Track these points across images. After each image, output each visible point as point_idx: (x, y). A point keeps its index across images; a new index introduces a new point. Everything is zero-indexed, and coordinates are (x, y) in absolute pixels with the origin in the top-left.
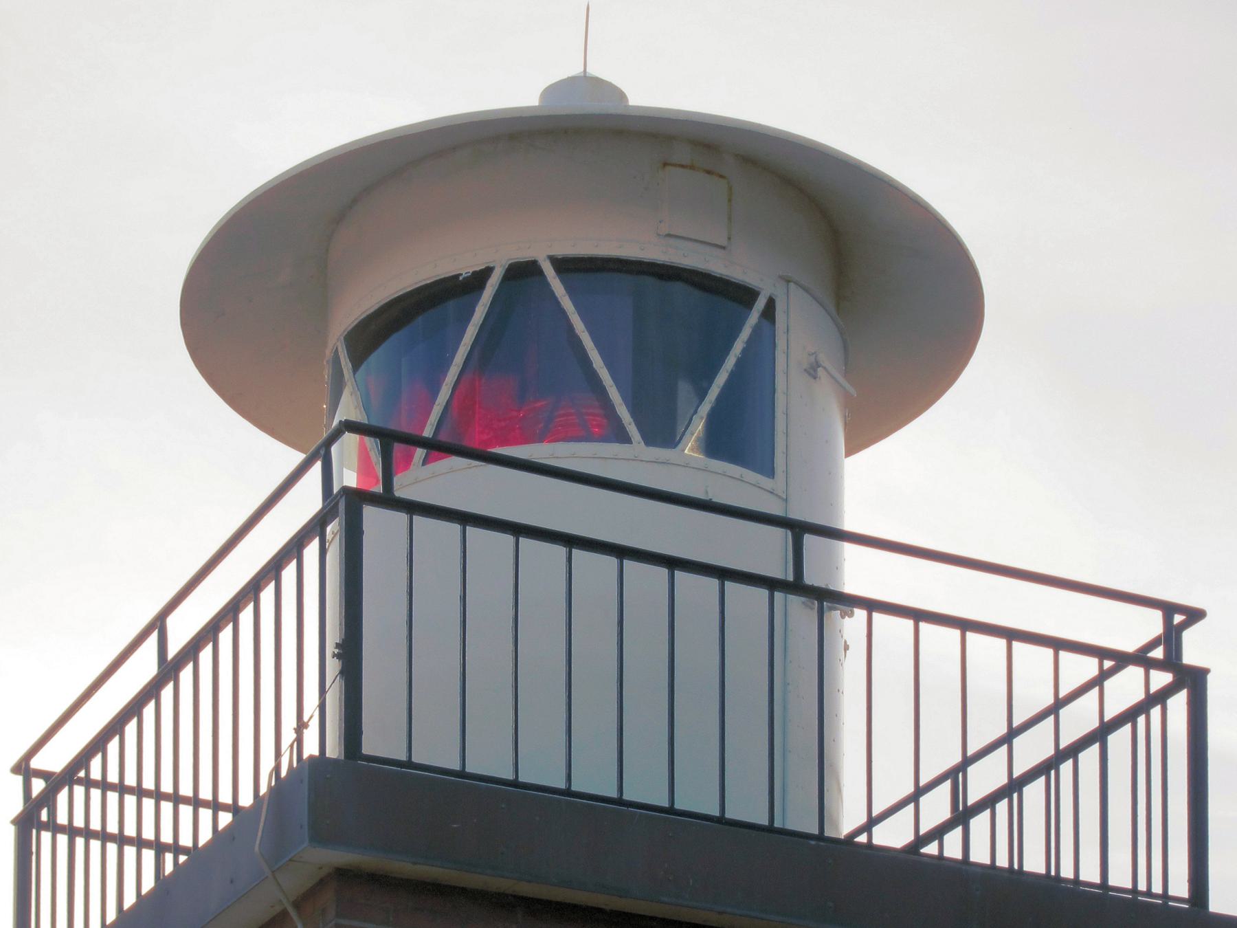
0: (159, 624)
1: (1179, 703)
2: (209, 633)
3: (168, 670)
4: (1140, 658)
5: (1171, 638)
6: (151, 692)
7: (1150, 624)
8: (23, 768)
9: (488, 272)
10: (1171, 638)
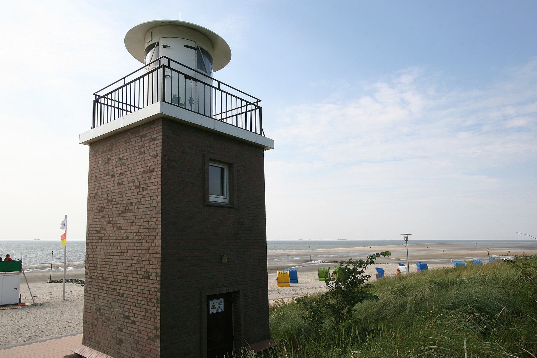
0: (124, 78)
1: (258, 111)
2: (130, 83)
3: (126, 85)
4: (253, 104)
5: (257, 102)
6: (122, 87)
7: (256, 100)
8: (95, 94)
9: (156, 43)
10: (257, 102)
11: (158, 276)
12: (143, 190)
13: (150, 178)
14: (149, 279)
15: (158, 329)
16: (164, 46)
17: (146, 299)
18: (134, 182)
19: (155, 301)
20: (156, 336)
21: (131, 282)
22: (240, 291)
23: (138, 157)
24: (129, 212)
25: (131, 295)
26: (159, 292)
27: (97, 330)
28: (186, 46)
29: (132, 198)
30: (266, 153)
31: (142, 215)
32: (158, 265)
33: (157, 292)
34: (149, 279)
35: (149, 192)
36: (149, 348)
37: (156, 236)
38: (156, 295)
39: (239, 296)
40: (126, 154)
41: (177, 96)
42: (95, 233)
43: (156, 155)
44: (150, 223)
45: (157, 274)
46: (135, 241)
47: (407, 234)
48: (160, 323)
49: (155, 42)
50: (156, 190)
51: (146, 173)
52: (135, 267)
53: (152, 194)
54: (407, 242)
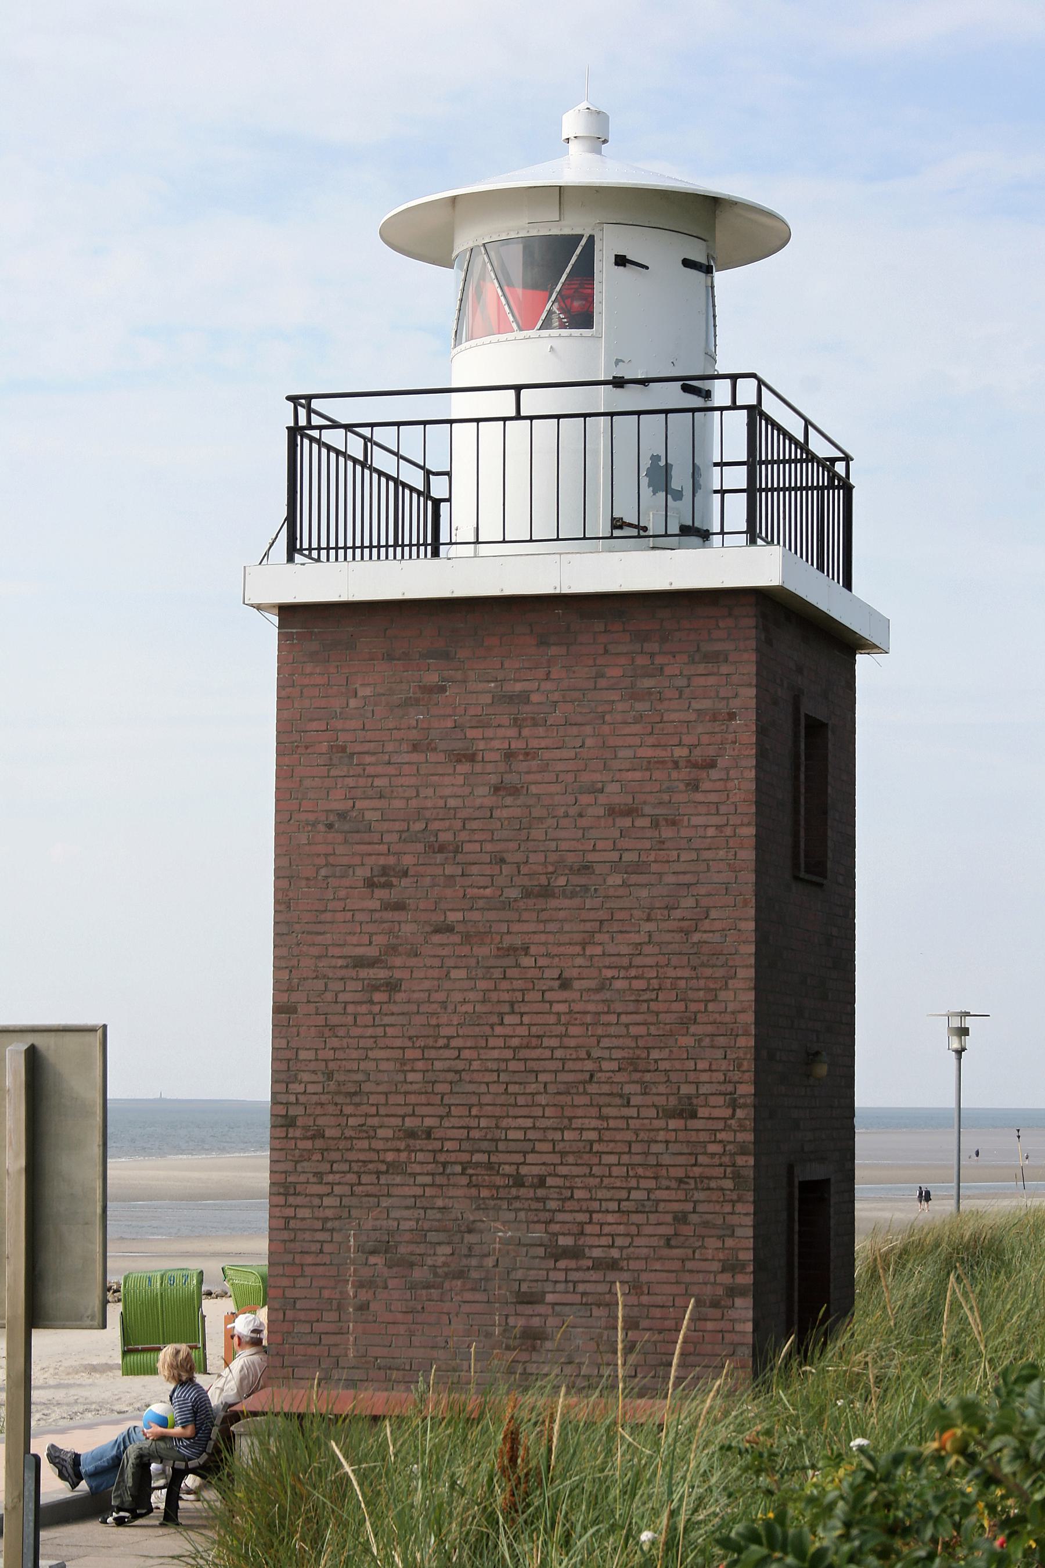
11: (744, 1106)
12: (655, 824)
13: (694, 786)
14: (694, 1115)
15: (743, 1266)
16: (621, 261)
17: (680, 1181)
18: (602, 791)
19: (728, 1184)
20: (732, 1292)
21: (593, 1135)
22: (832, 1181)
23: (620, 706)
24: (573, 895)
25: (594, 1176)
26: (749, 1154)
27: (375, 1322)
28: (687, 263)
29: (591, 848)
30: (862, 661)
31: (652, 909)
32: (744, 1072)
33: (735, 1153)
34: (694, 1115)
35: (684, 832)
36: (698, 1331)
37: (726, 979)
38: (734, 1165)
39: (239, 1338)
40: (548, 686)
41: (662, 463)
42: (347, 967)
43: (728, 714)
44: (696, 937)
45: (735, 1100)
46: (607, 995)
47: (968, 1014)
48: (754, 1249)
49: (577, 231)
50: (728, 831)
51: (670, 765)
52: (613, 1082)
53: (709, 840)
54: (959, 1059)
